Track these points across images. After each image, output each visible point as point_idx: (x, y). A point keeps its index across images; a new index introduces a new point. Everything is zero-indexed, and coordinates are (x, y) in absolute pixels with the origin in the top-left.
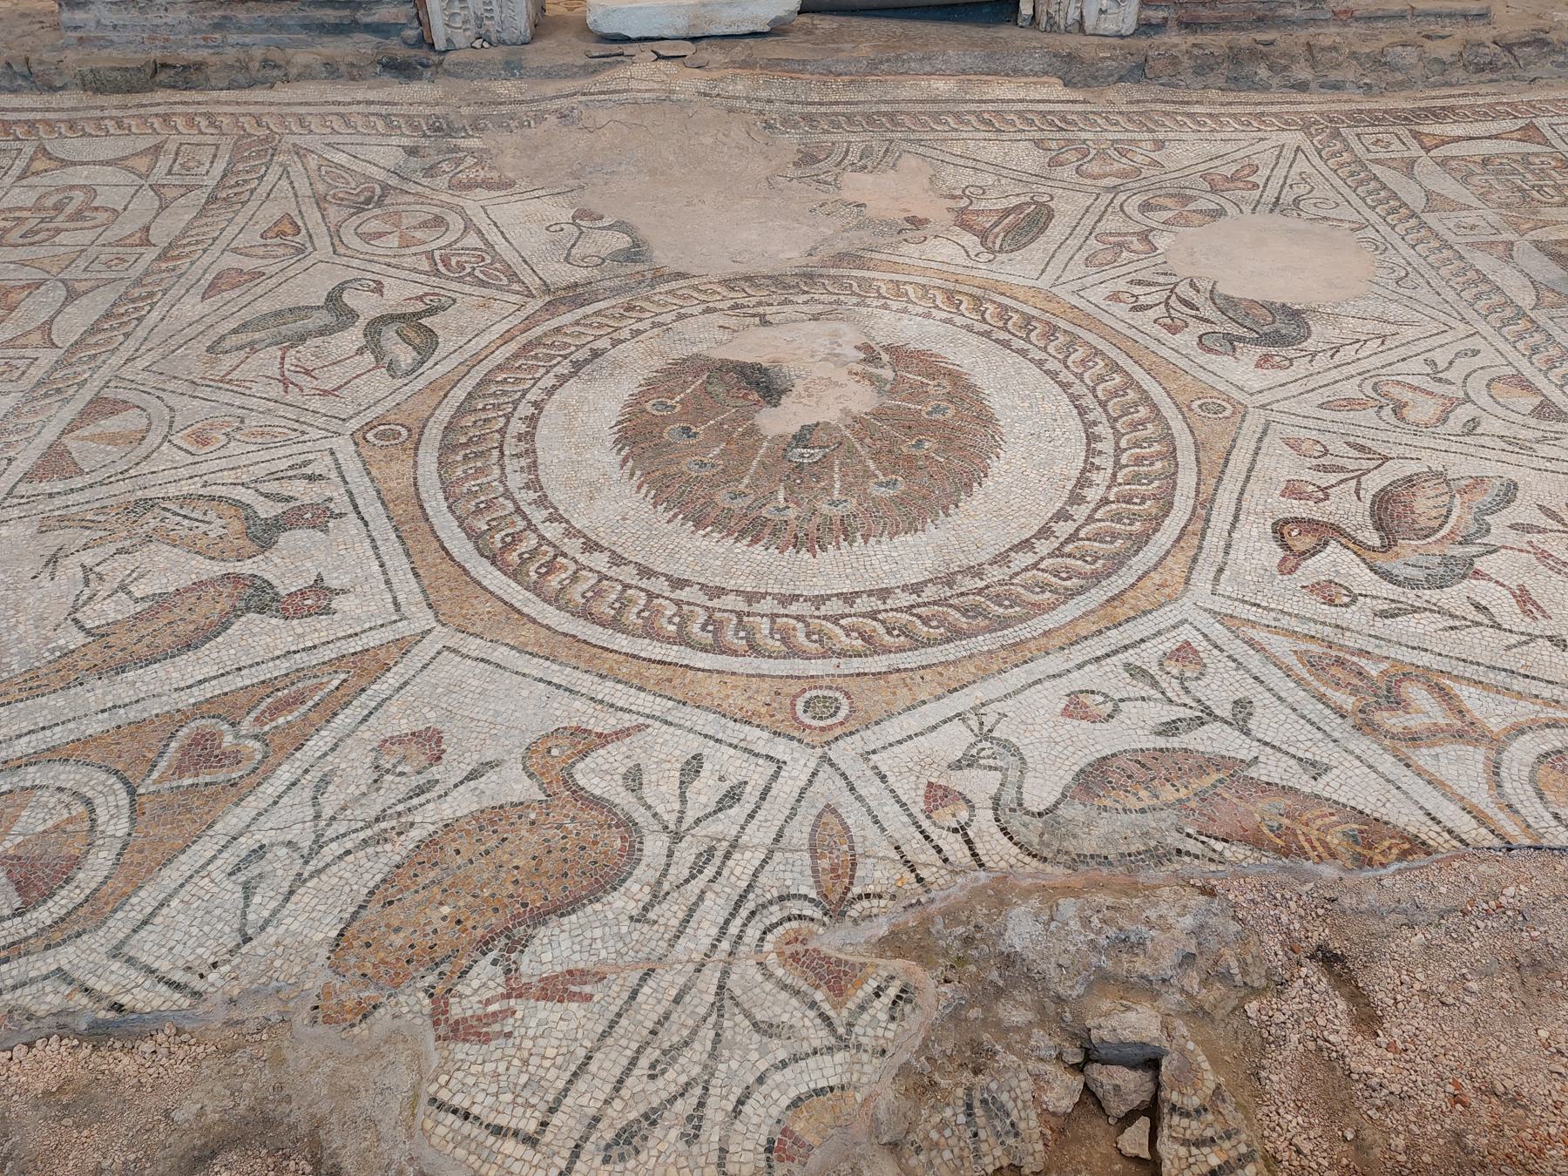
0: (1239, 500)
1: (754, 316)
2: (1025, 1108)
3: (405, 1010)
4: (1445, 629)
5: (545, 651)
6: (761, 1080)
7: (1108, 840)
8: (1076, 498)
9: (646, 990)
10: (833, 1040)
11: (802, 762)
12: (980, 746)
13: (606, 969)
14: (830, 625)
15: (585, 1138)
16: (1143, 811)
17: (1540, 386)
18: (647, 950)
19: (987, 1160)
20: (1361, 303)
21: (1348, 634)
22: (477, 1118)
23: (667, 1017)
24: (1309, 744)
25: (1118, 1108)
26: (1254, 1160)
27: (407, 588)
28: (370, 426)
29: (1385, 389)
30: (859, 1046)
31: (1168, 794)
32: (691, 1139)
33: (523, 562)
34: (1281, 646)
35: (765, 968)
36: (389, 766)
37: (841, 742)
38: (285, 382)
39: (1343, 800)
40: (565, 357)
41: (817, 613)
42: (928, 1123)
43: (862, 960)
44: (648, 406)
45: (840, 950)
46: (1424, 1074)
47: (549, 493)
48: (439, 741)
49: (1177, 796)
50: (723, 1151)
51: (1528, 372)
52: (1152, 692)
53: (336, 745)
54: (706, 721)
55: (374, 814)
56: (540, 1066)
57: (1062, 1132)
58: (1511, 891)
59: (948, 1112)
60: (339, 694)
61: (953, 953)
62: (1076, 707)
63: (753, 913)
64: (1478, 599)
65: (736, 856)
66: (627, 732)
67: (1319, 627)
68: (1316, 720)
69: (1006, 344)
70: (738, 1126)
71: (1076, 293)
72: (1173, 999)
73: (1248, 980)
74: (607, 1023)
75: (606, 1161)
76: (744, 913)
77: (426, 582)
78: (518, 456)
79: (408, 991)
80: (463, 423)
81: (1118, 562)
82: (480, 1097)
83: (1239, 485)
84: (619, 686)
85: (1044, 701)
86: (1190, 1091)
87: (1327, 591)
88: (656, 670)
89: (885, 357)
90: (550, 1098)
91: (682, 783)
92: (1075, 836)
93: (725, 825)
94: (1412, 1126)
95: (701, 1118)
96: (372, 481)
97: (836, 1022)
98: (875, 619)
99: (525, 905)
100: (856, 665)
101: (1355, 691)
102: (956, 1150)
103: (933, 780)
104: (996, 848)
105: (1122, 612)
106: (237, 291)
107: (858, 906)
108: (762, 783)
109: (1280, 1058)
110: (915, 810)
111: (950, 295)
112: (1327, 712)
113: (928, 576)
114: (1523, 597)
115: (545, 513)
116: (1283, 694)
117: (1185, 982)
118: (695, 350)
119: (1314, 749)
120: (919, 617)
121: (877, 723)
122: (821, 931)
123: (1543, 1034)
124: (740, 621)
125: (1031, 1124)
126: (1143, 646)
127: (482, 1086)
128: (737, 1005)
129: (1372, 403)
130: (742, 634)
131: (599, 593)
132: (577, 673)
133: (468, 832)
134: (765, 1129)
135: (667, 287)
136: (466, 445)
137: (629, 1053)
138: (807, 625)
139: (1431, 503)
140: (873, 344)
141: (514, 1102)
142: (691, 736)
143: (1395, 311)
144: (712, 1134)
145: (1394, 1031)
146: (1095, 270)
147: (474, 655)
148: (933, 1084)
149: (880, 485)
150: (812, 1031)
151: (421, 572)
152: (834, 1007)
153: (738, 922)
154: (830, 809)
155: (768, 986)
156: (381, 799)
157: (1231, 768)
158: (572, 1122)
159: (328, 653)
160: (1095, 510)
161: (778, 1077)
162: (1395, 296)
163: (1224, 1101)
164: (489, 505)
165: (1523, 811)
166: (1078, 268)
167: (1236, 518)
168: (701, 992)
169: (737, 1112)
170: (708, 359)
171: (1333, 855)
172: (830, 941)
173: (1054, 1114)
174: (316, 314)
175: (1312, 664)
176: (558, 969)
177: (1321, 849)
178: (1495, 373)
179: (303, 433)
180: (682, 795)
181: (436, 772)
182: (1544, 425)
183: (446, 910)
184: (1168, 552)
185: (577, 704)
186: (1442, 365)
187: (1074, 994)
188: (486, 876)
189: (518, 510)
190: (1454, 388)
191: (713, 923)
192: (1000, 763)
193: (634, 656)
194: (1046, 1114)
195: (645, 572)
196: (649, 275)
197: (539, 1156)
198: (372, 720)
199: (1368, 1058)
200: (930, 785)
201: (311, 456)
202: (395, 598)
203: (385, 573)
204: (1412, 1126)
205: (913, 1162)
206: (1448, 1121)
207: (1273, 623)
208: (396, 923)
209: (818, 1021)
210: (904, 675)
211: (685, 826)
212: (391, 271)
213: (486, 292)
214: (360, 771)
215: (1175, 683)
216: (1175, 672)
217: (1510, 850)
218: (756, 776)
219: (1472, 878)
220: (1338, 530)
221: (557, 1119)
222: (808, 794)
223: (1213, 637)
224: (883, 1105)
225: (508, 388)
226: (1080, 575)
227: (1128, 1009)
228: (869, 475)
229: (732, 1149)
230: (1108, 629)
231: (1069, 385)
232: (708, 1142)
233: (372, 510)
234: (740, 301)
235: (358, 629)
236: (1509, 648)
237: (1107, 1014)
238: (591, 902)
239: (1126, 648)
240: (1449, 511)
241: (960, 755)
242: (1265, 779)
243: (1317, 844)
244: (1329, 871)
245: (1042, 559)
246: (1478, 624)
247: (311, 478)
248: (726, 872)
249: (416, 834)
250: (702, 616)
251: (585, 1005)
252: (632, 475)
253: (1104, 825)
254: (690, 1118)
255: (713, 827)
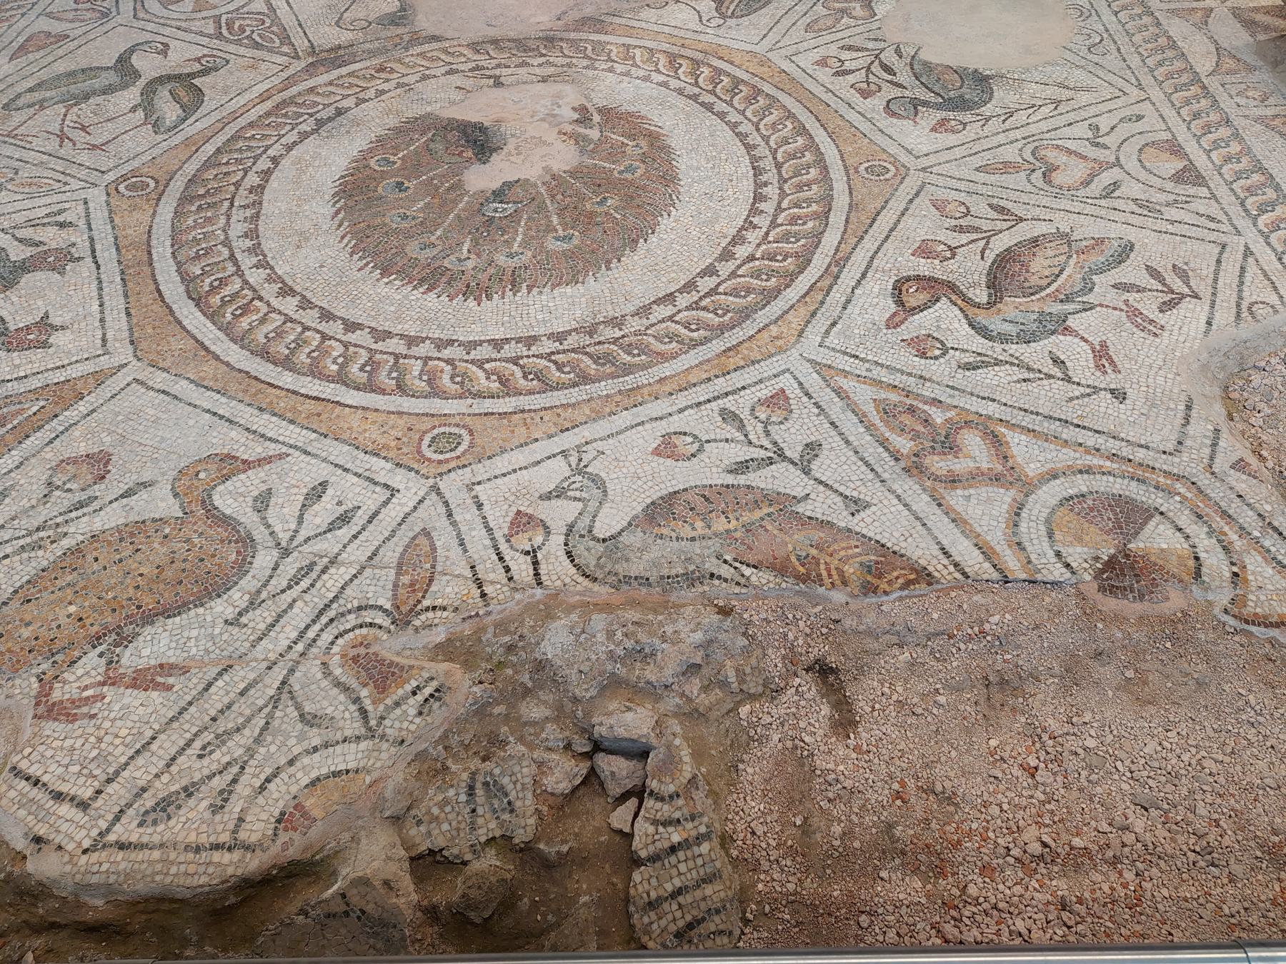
0: (872, 258)
1: (490, 77)
2: (523, 789)
3: (17, 691)
4: (1018, 381)
5: (219, 386)
6: (291, 763)
7: (655, 564)
8: (726, 255)
9: (220, 683)
10: (363, 730)
11: (413, 491)
12: (573, 479)
13: (192, 664)
14: (474, 368)
15: (129, 805)
16: (693, 539)
17: (1188, 150)
18: (231, 649)
19: (481, 831)
20: (1049, 68)
21: (928, 384)
22: (44, 785)
23: (229, 707)
24: (859, 483)
25: (615, 790)
26: (710, 839)
27: (118, 325)
28: (124, 178)
29: (1043, 153)
30: (383, 737)
31: (720, 524)
32: (216, 809)
33: (224, 303)
34: (864, 395)
35: (327, 668)
36: (59, 483)
37: (452, 474)
38: (62, 137)
39: (871, 534)
40: (311, 115)
41: (466, 357)
42: (433, 798)
43: (412, 662)
44: (372, 163)
45: (398, 654)
46: (876, 773)
47: (263, 242)
48: (108, 462)
49: (727, 526)
50: (241, 820)
51: (1183, 136)
52: (737, 434)
53: (21, 463)
54: (339, 452)
55: (36, 524)
56: (112, 743)
57: (561, 808)
58: (996, 619)
59: (451, 792)
60: (34, 419)
61: (495, 659)
62: (666, 448)
63: (332, 620)
64: (1059, 354)
65: (332, 571)
66: (269, 460)
67: (904, 377)
68: (872, 462)
69: (709, 107)
70: (261, 800)
71: (789, 58)
72: (672, 702)
73: (744, 687)
74: (177, 710)
75: (140, 825)
76: (324, 620)
77: (135, 321)
78: (244, 207)
79: (24, 676)
80: (206, 176)
81: (745, 314)
82: (53, 767)
83: (877, 244)
84: (274, 419)
85: (641, 441)
86: (668, 779)
87: (922, 347)
88: (310, 406)
89: (597, 118)
90: (111, 770)
91: (304, 505)
92: (627, 560)
93: (329, 545)
94: (853, 817)
95: (230, 792)
96: (113, 228)
97: (371, 715)
98: (516, 364)
99: (139, 607)
100: (488, 405)
101: (916, 436)
102: (454, 823)
103: (522, 509)
104: (557, 568)
105: (735, 360)
106: (42, 53)
107: (423, 617)
108: (373, 508)
109: (759, 754)
110: (498, 535)
111: (673, 59)
112: (885, 455)
113: (574, 325)
114: (1102, 355)
115: (254, 260)
116: (851, 439)
117: (687, 688)
118: (429, 109)
119: (862, 489)
120: (555, 363)
121: (490, 458)
122: (385, 637)
123: (993, 743)
124: (396, 362)
125: (527, 803)
126: (742, 393)
127: (57, 758)
128: (292, 698)
129: (1027, 166)
130: (394, 375)
131: (279, 334)
132: (241, 406)
133: (110, 543)
134: (281, 804)
135: (418, 50)
136: (203, 196)
137: (188, 736)
138: (455, 368)
139: (1048, 262)
140: (589, 106)
141: (80, 772)
142: (324, 465)
143: (1079, 77)
144: (235, 807)
145: (864, 735)
146: (813, 35)
147: (157, 387)
148: (446, 768)
149: (557, 239)
150: (348, 722)
151: (132, 311)
152: (374, 703)
153: (317, 627)
154: (426, 533)
155: (325, 683)
156: (46, 512)
157: (782, 504)
158: (122, 792)
159: (35, 383)
160: (739, 267)
161: (306, 760)
162: (1083, 62)
163: (697, 788)
164: (208, 251)
165: (1029, 549)
166: (798, 33)
167: (864, 275)
168: (266, 686)
169: (263, 788)
170: (437, 117)
171: (845, 583)
172: (390, 646)
173: (552, 794)
174: (104, 74)
175: (887, 411)
176: (153, 662)
177: (836, 577)
178: (1149, 138)
179: (66, 184)
180: (301, 517)
181: (97, 490)
182: (1180, 189)
183: (72, 609)
184: (792, 306)
185: (233, 434)
186: (1104, 130)
187: (588, 695)
188: (113, 581)
189: (232, 257)
190: (1107, 152)
191: (296, 627)
192: (584, 495)
193: (294, 392)
194: (541, 794)
195: (327, 316)
196: (406, 38)
197: (87, 818)
198: (57, 442)
199: (837, 759)
200: (519, 512)
201: (67, 205)
202: (104, 335)
203: (102, 312)
204: (853, 817)
205: (413, 832)
206: (885, 814)
207: (864, 374)
208: (28, 618)
209: (357, 714)
210: (526, 415)
211: (295, 543)
212: (180, 34)
213: (257, 53)
214: (35, 487)
215: (760, 426)
216: (763, 416)
217: (1006, 582)
218: (370, 502)
219: (965, 606)
220: (952, 287)
221: (110, 789)
222: (410, 518)
223: (806, 385)
224: (391, 785)
225: (253, 144)
226: (708, 327)
227: (629, 709)
228: (550, 229)
229: (248, 819)
230: (717, 377)
231: (755, 147)
232: (231, 812)
233: (107, 255)
234: (480, 64)
235: (66, 362)
236: (1071, 399)
237: (610, 714)
238: (196, 606)
239: (727, 394)
240: (1061, 271)
241: (552, 486)
242: (808, 513)
243: (834, 572)
244: (838, 596)
245: (680, 311)
246: (1049, 376)
247: (62, 225)
248: (318, 585)
249: (66, 543)
250: (364, 356)
251: (164, 694)
252: (340, 226)
253: (654, 553)
254: (221, 792)
255: (319, 546)
